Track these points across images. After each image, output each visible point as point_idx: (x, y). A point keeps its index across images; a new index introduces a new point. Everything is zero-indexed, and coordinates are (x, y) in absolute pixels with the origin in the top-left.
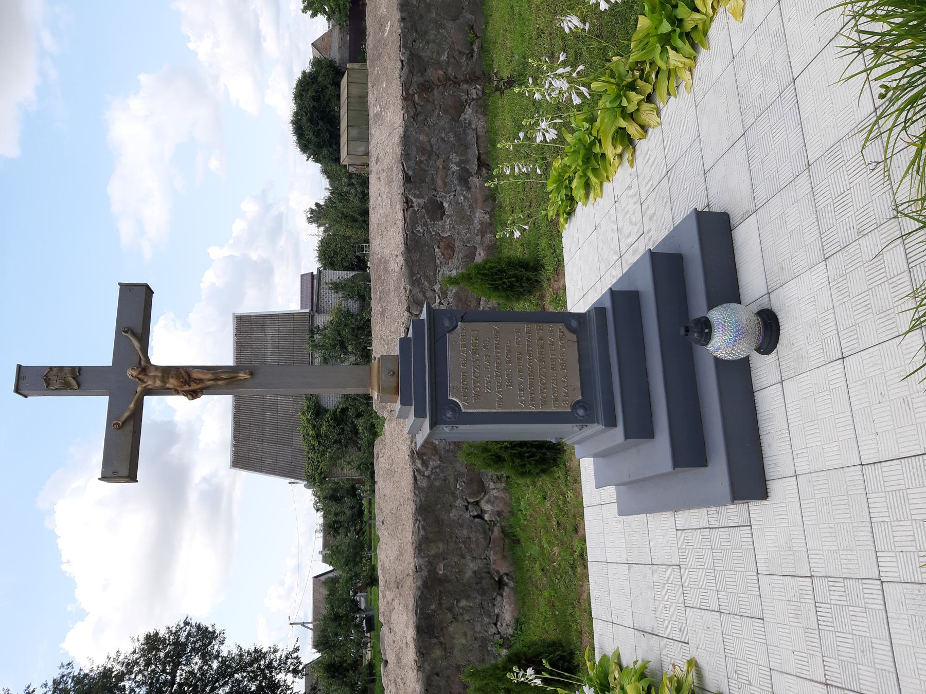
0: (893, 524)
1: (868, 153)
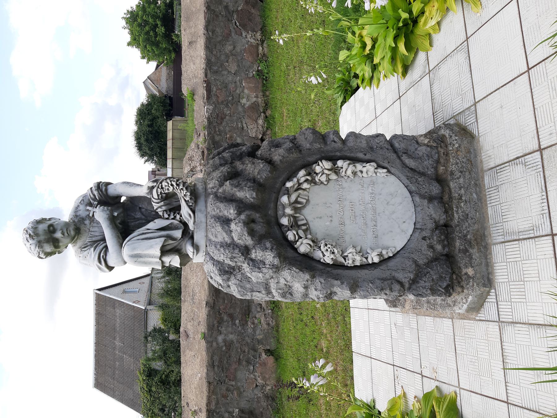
0: (533, 348)
1: (533, 73)
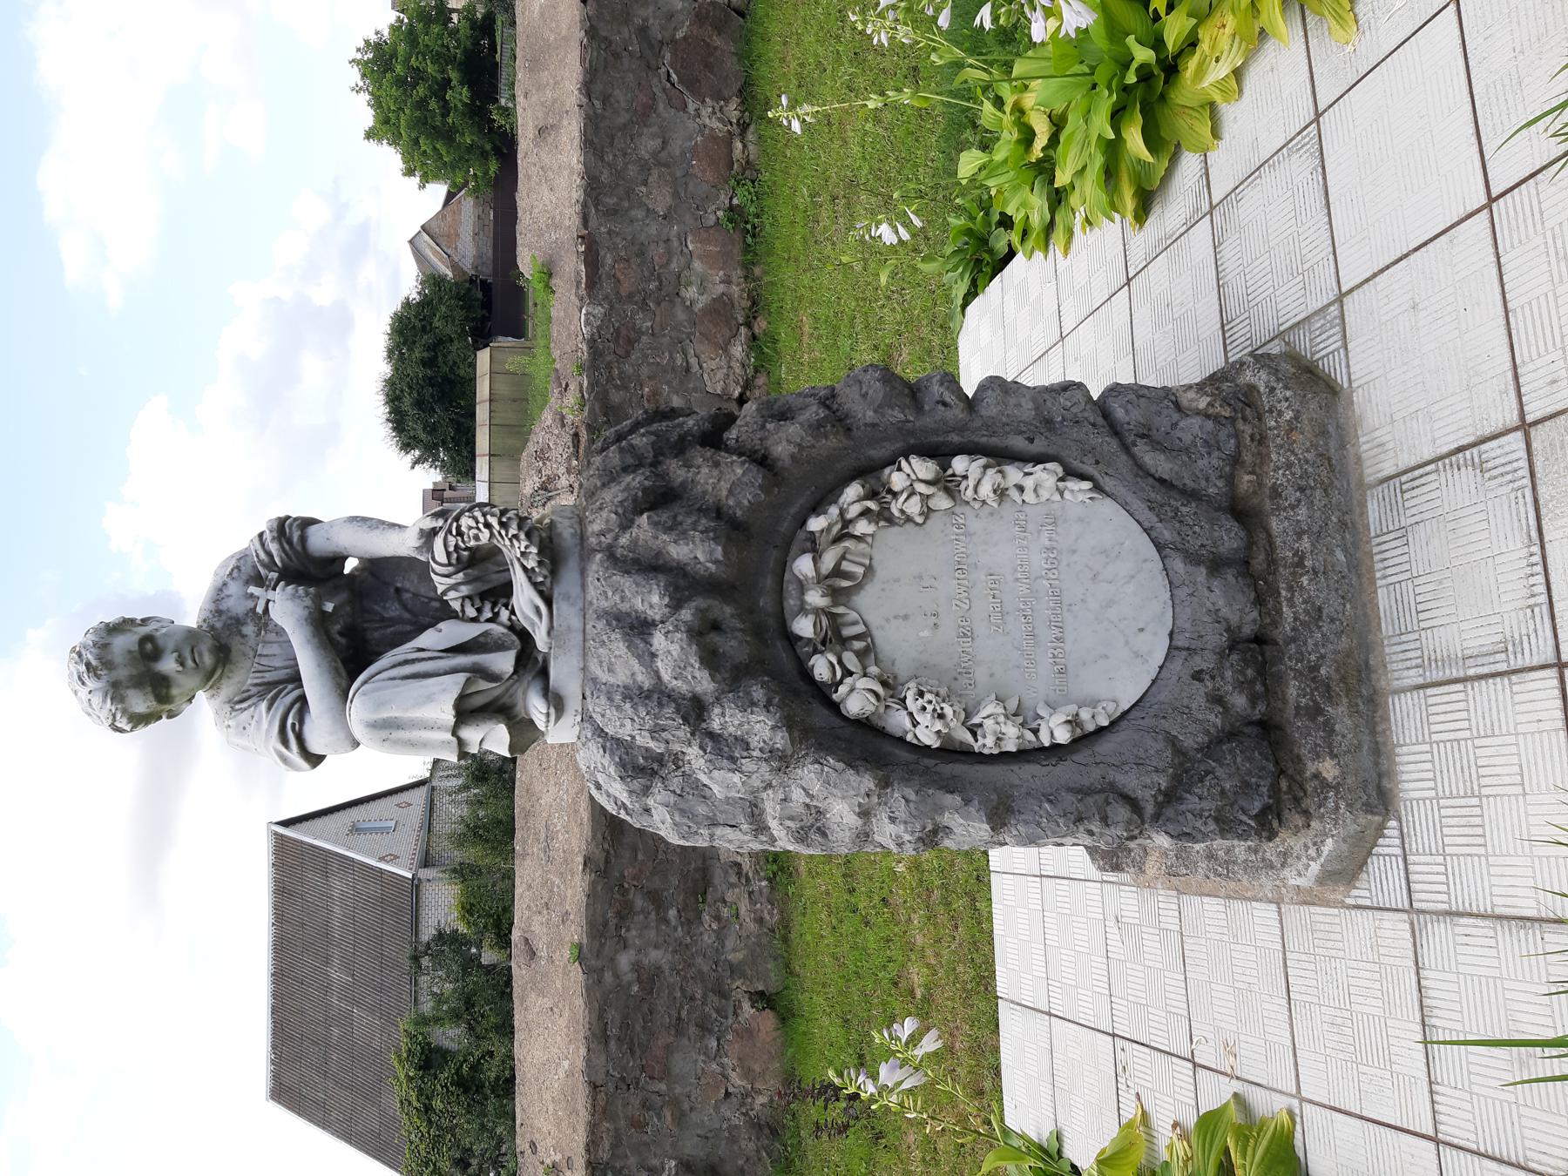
0: (1507, 984)
